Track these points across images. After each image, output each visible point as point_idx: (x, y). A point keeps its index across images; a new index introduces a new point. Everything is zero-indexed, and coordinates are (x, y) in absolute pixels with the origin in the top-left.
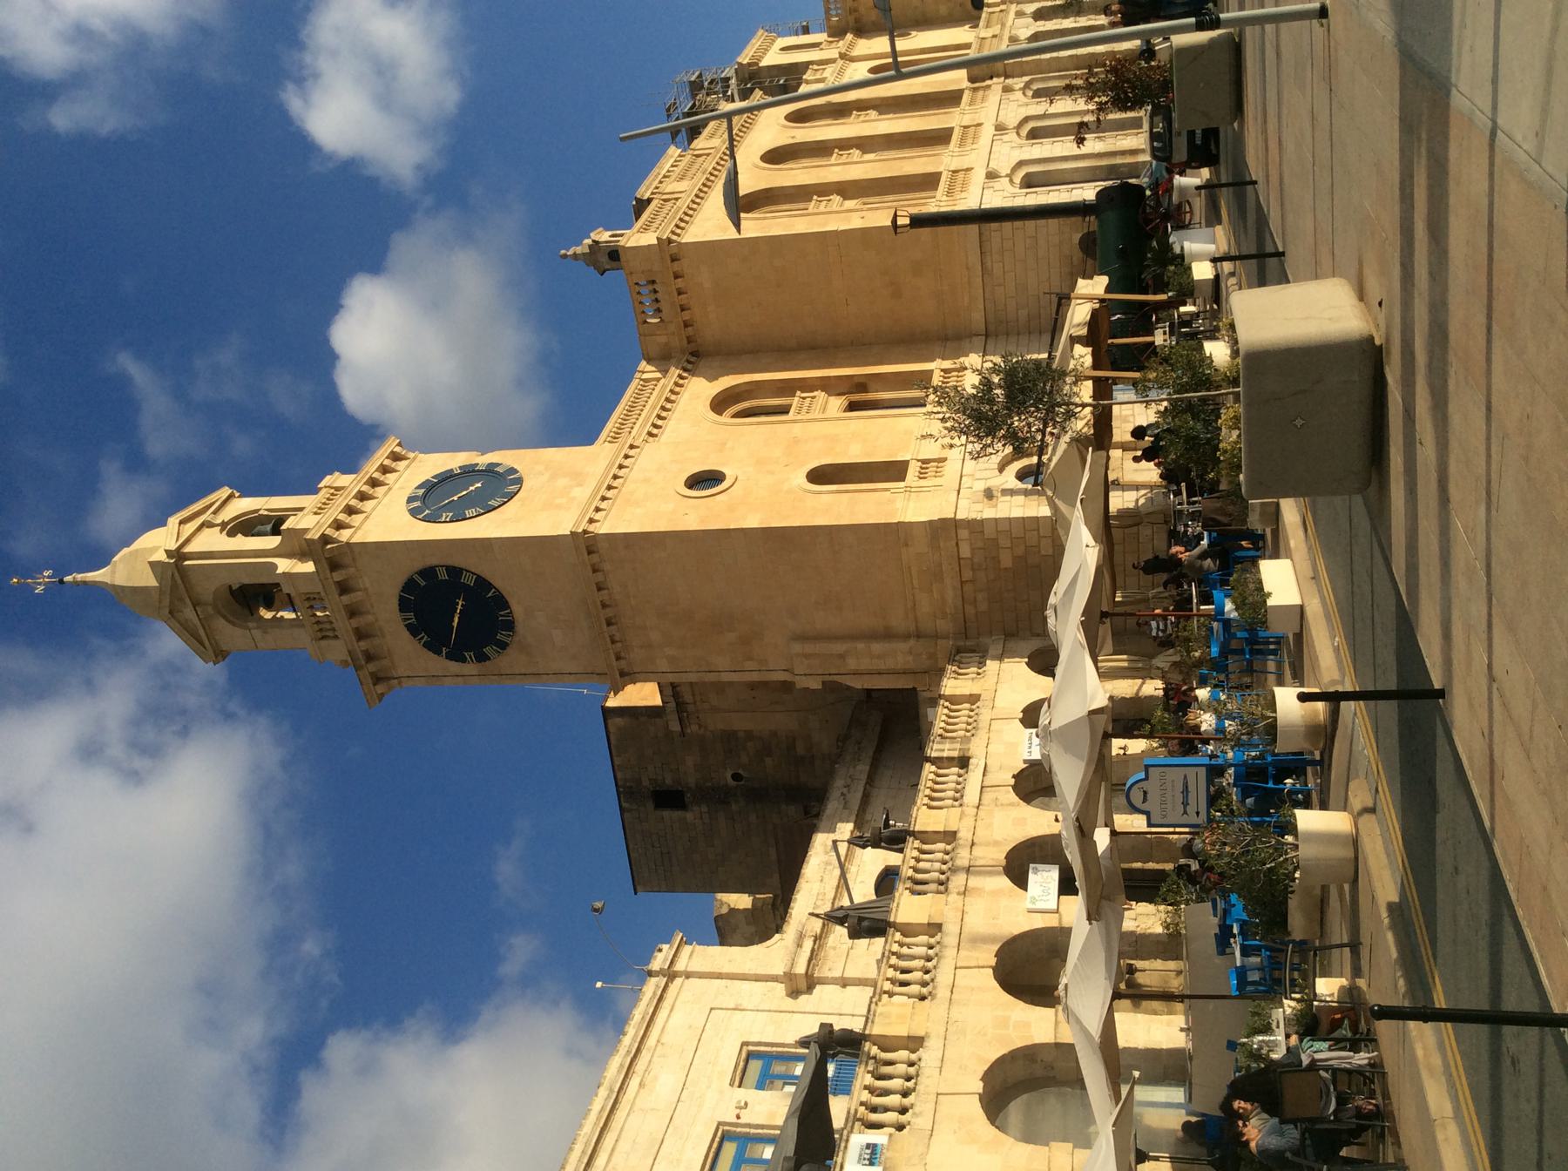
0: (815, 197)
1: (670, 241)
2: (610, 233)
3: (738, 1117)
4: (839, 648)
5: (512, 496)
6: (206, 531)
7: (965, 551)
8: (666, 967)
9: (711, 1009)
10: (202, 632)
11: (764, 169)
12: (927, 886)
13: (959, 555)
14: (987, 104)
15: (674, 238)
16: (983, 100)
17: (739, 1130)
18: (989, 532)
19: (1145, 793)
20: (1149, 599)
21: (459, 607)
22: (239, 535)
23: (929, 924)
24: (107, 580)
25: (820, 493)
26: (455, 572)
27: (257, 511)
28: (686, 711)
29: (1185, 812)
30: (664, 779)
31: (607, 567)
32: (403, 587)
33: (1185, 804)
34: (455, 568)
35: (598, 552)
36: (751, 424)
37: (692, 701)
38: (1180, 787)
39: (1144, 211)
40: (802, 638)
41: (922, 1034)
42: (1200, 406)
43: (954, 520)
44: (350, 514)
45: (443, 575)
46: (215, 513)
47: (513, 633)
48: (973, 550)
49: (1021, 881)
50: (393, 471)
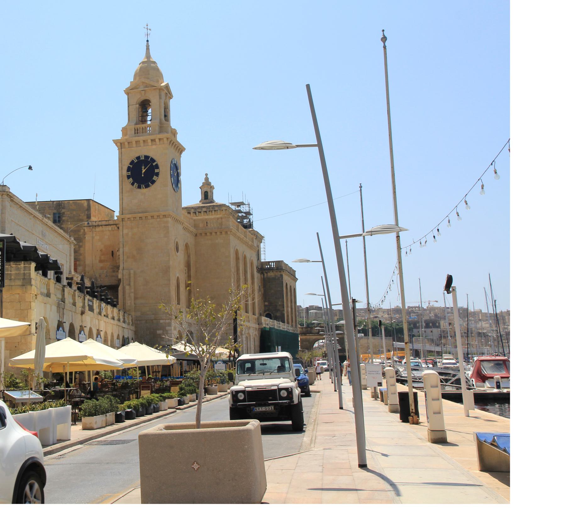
13: (161, 319)
30: (64, 217)
32: (153, 158)
37: (96, 230)
42: (157, 401)
45: (156, 171)
47: (137, 188)
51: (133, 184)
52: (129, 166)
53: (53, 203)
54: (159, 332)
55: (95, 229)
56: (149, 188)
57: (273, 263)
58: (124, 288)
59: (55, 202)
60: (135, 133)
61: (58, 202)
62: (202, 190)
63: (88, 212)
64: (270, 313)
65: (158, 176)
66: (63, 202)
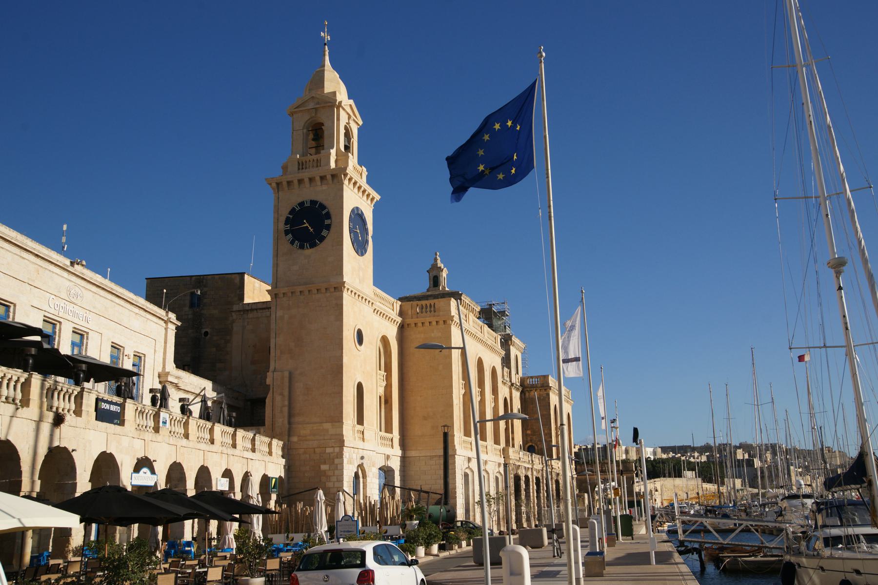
0: (464, 382)
1: (452, 321)
2: (446, 277)
3: (126, 355)
4: (286, 393)
5: (357, 253)
6: (347, 116)
7: (328, 450)
8: (171, 320)
9: (155, 340)
10: (301, 109)
11: (476, 358)
12: (57, 400)
14: (494, 456)
15: (453, 323)
16: (496, 454)
17: (121, 356)
18: (337, 461)
19: (348, 520)
20: (844, 506)
21: (310, 228)
22: (345, 131)
23: (214, 439)
24: (326, 68)
25: (354, 388)
26: (328, 227)
27: (353, 137)
28: (244, 314)
29: (341, 531)
30: (206, 298)
31: (328, 294)
32: (322, 204)
33: (344, 531)
34: (330, 228)
35: (335, 292)
36: (376, 353)
38: (350, 530)
39: (210, 546)
40: (291, 375)
41: (190, 439)
43: (344, 446)
44: (349, 179)
45: (327, 222)
46: (354, 120)
48: (329, 453)
49: (224, 476)
50: (367, 199)
51: (292, 243)
52: (287, 217)
53: (191, 279)
54: (324, 467)
55: (247, 315)
56: (315, 248)
57: (537, 379)
58: (273, 399)
59: (194, 277)
60: (299, 169)
61: (199, 277)
62: (431, 275)
63: (240, 292)
64: (534, 445)
65: (329, 230)
66: (205, 277)
